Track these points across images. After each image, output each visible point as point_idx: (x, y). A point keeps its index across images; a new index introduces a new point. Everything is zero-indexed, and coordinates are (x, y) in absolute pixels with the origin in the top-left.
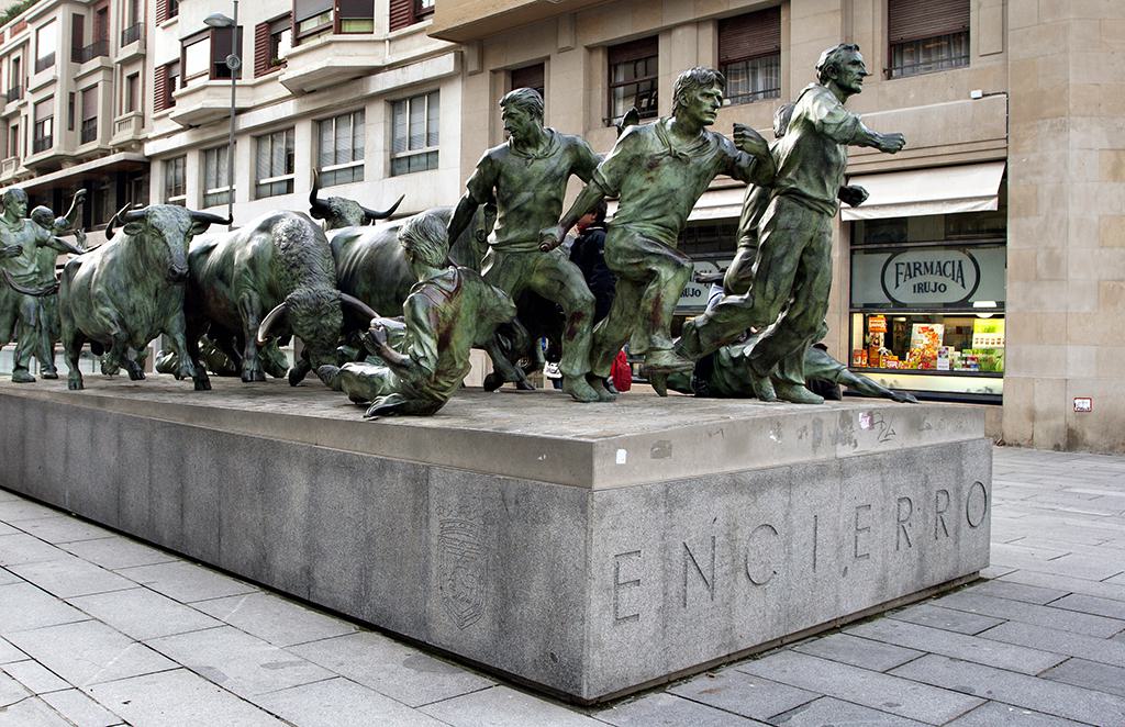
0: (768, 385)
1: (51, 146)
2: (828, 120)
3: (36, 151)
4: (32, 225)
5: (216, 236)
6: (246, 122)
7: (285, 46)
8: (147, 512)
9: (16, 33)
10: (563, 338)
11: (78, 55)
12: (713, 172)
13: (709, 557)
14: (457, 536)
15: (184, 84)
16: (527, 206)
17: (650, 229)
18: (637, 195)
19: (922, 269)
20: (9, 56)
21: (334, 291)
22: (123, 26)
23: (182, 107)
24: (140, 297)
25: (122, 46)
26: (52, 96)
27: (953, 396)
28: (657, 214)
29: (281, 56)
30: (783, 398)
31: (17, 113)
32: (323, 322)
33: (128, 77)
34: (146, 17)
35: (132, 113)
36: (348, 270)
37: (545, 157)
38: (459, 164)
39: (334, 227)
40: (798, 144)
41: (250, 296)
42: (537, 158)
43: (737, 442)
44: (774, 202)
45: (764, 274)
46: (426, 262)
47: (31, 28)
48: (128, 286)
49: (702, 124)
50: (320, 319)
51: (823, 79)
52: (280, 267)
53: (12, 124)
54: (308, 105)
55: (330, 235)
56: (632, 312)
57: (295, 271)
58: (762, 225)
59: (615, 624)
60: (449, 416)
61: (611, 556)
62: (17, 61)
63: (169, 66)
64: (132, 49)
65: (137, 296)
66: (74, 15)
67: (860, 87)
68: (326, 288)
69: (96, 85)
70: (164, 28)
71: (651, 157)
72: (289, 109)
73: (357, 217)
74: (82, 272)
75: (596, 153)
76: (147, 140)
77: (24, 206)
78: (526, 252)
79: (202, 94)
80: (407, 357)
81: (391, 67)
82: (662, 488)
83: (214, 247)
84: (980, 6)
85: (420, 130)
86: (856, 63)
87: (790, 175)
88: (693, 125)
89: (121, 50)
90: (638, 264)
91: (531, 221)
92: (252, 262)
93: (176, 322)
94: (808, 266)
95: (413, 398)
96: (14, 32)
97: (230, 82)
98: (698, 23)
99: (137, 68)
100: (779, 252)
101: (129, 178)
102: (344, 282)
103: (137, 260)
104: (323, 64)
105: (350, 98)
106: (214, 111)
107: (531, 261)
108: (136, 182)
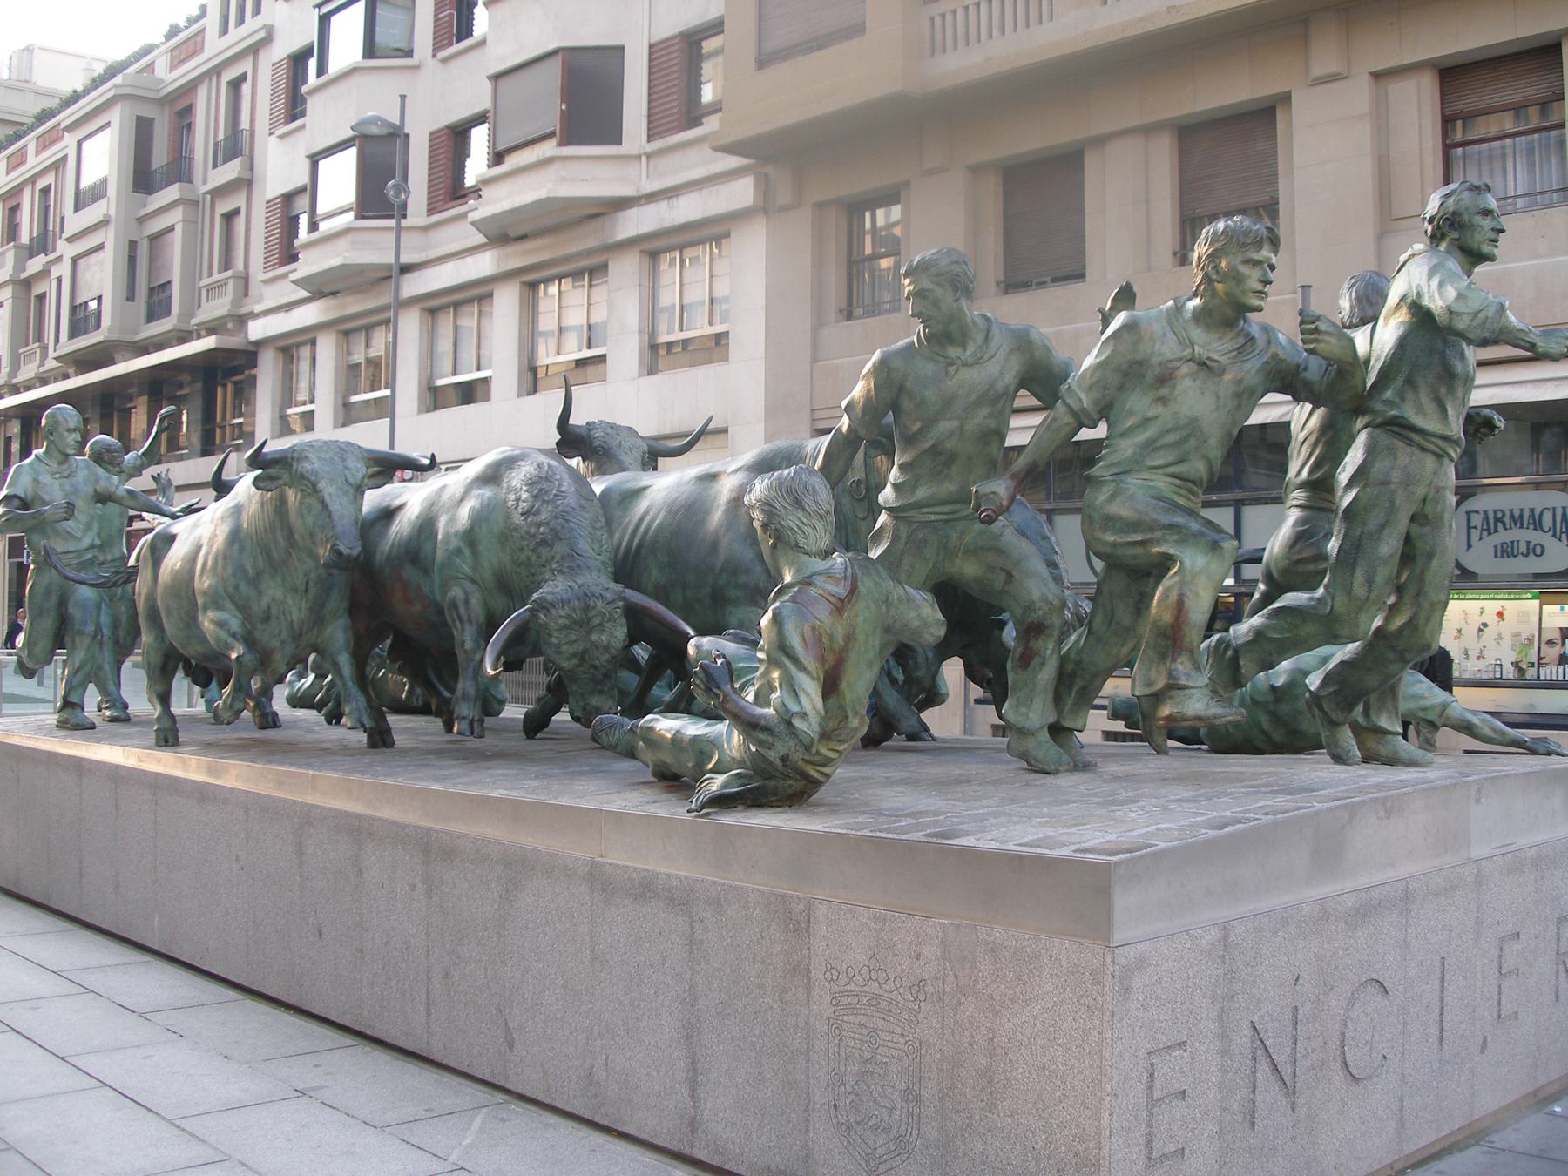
0: (1347, 738)
1: (98, 326)
2: (1456, 308)
3: (74, 333)
4: (88, 467)
5: (412, 497)
6: (414, 286)
7: (476, 167)
9: (45, 147)
10: (1009, 665)
11: (143, 179)
12: (1260, 389)
13: (1288, 1041)
14: (863, 1020)
15: (313, 226)
16: (949, 445)
17: (1161, 483)
18: (1138, 426)
19: (1507, 520)
20: (34, 183)
21: (612, 585)
22: (216, 135)
23: (309, 264)
24: (279, 594)
25: (215, 166)
26: (101, 247)
27: (1539, 720)
28: (1170, 459)
29: (470, 181)
30: (1369, 758)
31: (44, 273)
32: (594, 637)
33: (223, 215)
34: (252, 121)
35: (229, 273)
37: (977, 361)
39: (601, 470)
40: (1402, 345)
41: (466, 593)
42: (965, 365)
43: (1327, 845)
44: (1362, 439)
45: (1352, 552)
46: (797, 547)
47: (70, 140)
48: (259, 574)
49: (1243, 309)
50: (589, 632)
51: (1436, 238)
52: (518, 548)
53: (37, 291)
54: (515, 257)
55: (598, 487)
56: (1127, 620)
57: (544, 552)
58: (1343, 477)
59: (1147, 1167)
60: (833, 809)
61: (1142, 1054)
62: (46, 191)
63: (288, 198)
64: (230, 171)
65: (273, 591)
66: (138, 118)
67: (1496, 252)
68: (600, 582)
69: (171, 229)
70: (281, 137)
71: (1161, 364)
72: (484, 265)
73: (637, 454)
74: (175, 558)
75: (1061, 354)
76: (254, 316)
77: (77, 436)
78: (947, 521)
79: (343, 243)
80: (771, 711)
81: (652, 197)
82: (1215, 933)
83: (401, 507)
85: (698, 293)
86: (1487, 213)
87: (1388, 394)
88: (1229, 312)
89: (212, 173)
90: (1142, 543)
91: (954, 469)
92: (470, 537)
93: (338, 634)
94: (1419, 544)
95: (772, 777)
96: (44, 143)
97: (392, 223)
98: (1148, 130)
99: (238, 201)
100: (1373, 523)
101: (221, 378)
102: (626, 568)
103: (273, 532)
104: (541, 194)
105: (581, 248)
106: (360, 269)
107: (954, 536)
108: (235, 383)
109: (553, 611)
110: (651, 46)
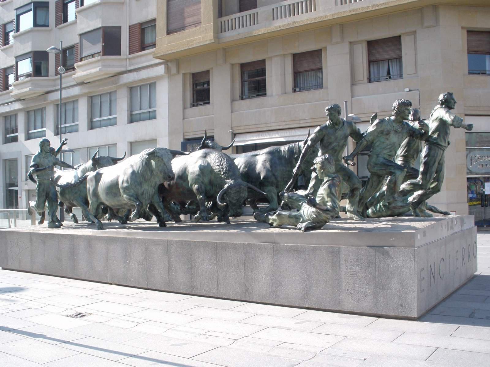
8: (168, 279)
32: (241, 195)
36: (140, 171)
38: (167, 117)
84: (406, 54)
109: (233, 189)
110: (129, 26)
